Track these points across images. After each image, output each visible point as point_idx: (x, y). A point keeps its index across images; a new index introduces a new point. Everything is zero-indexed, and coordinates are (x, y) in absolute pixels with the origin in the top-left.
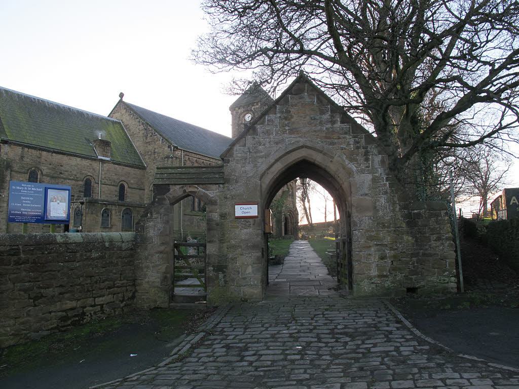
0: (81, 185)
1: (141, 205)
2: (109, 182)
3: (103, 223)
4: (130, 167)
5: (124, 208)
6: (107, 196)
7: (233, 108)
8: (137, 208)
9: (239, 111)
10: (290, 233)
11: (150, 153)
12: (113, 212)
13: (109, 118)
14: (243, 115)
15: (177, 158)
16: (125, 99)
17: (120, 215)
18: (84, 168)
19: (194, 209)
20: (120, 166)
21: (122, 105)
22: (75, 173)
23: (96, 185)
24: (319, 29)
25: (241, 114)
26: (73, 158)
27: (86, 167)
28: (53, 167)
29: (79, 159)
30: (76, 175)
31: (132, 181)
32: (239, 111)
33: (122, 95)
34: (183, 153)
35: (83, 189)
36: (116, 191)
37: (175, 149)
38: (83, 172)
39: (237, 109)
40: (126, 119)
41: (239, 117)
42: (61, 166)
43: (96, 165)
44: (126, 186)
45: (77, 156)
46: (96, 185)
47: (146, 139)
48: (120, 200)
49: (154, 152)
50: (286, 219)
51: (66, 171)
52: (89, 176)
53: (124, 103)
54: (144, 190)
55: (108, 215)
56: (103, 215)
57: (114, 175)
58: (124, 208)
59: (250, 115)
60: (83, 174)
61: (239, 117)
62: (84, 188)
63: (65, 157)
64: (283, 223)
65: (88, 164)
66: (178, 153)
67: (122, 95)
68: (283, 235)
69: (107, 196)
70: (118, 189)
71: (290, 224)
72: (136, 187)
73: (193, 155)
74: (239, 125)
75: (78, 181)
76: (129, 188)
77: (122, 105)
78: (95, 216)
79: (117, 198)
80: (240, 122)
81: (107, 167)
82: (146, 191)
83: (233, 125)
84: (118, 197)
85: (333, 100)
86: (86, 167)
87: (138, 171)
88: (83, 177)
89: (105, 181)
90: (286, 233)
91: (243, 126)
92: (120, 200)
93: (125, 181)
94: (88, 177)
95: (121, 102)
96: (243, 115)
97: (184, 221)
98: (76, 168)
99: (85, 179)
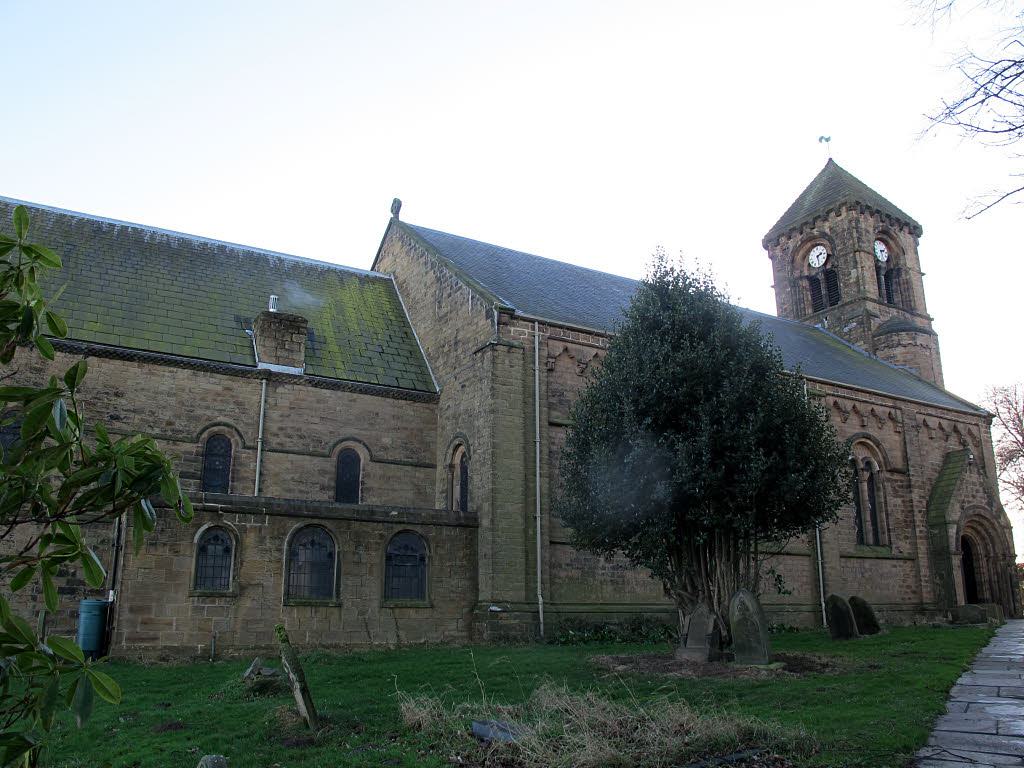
0: (191, 453)
1: (373, 512)
2: (297, 445)
3: (199, 579)
4: (378, 393)
5: (296, 525)
6: (290, 491)
7: (771, 242)
8: (356, 525)
9: (791, 244)
10: (987, 595)
11: (446, 349)
12: (250, 539)
13: (374, 274)
14: (801, 253)
15: (511, 346)
16: (405, 217)
17: (280, 550)
18: (203, 399)
19: (862, 539)
20: (339, 393)
21: (400, 234)
22: (167, 415)
23: (244, 455)
24: (994, 407)
25: (796, 250)
26: (165, 371)
27: (210, 398)
28: (89, 397)
29: (187, 372)
30: (170, 423)
31: (386, 441)
32: (791, 244)
33: (397, 206)
34: (537, 333)
35: (196, 467)
36: (323, 472)
37: (506, 318)
38: (199, 412)
39: (783, 239)
40: (405, 268)
41: (793, 261)
42: (117, 395)
43: (252, 393)
44: (362, 457)
45: (176, 364)
46: (244, 455)
47: (440, 307)
48: (337, 500)
49: (456, 343)
50: (966, 544)
51: (134, 411)
52: (218, 424)
53: (405, 227)
54: (434, 466)
55: (227, 550)
56: (202, 549)
57: (317, 420)
58: (296, 525)
59: (820, 249)
60: (197, 419)
61: (793, 261)
62: (199, 466)
63: (133, 369)
64: (956, 561)
65: (219, 388)
66: (519, 332)
67: (397, 206)
68: (961, 599)
69: (290, 491)
70: (330, 465)
71: (983, 562)
72: (398, 457)
73: (582, 339)
74: (794, 284)
75: (176, 441)
76: (373, 460)
77: (400, 234)
78: (166, 552)
79: (326, 496)
80: (797, 274)
81: (292, 398)
82: (440, 468)
83: (778, 285)
84: (332, 493)
85: (1000, 489)
86: (210, 398)
87: (408, 409)
88: (198, 430)
89: (282, 439)
90: (973, 596)
91: (805, 283)
92: (337, 500)
93: (360, 442)
94: (216, 429)
95: (395, 225)
96: (801, 253)
97: (552, 565)
98: (172, 401)
99: (205, 435)
